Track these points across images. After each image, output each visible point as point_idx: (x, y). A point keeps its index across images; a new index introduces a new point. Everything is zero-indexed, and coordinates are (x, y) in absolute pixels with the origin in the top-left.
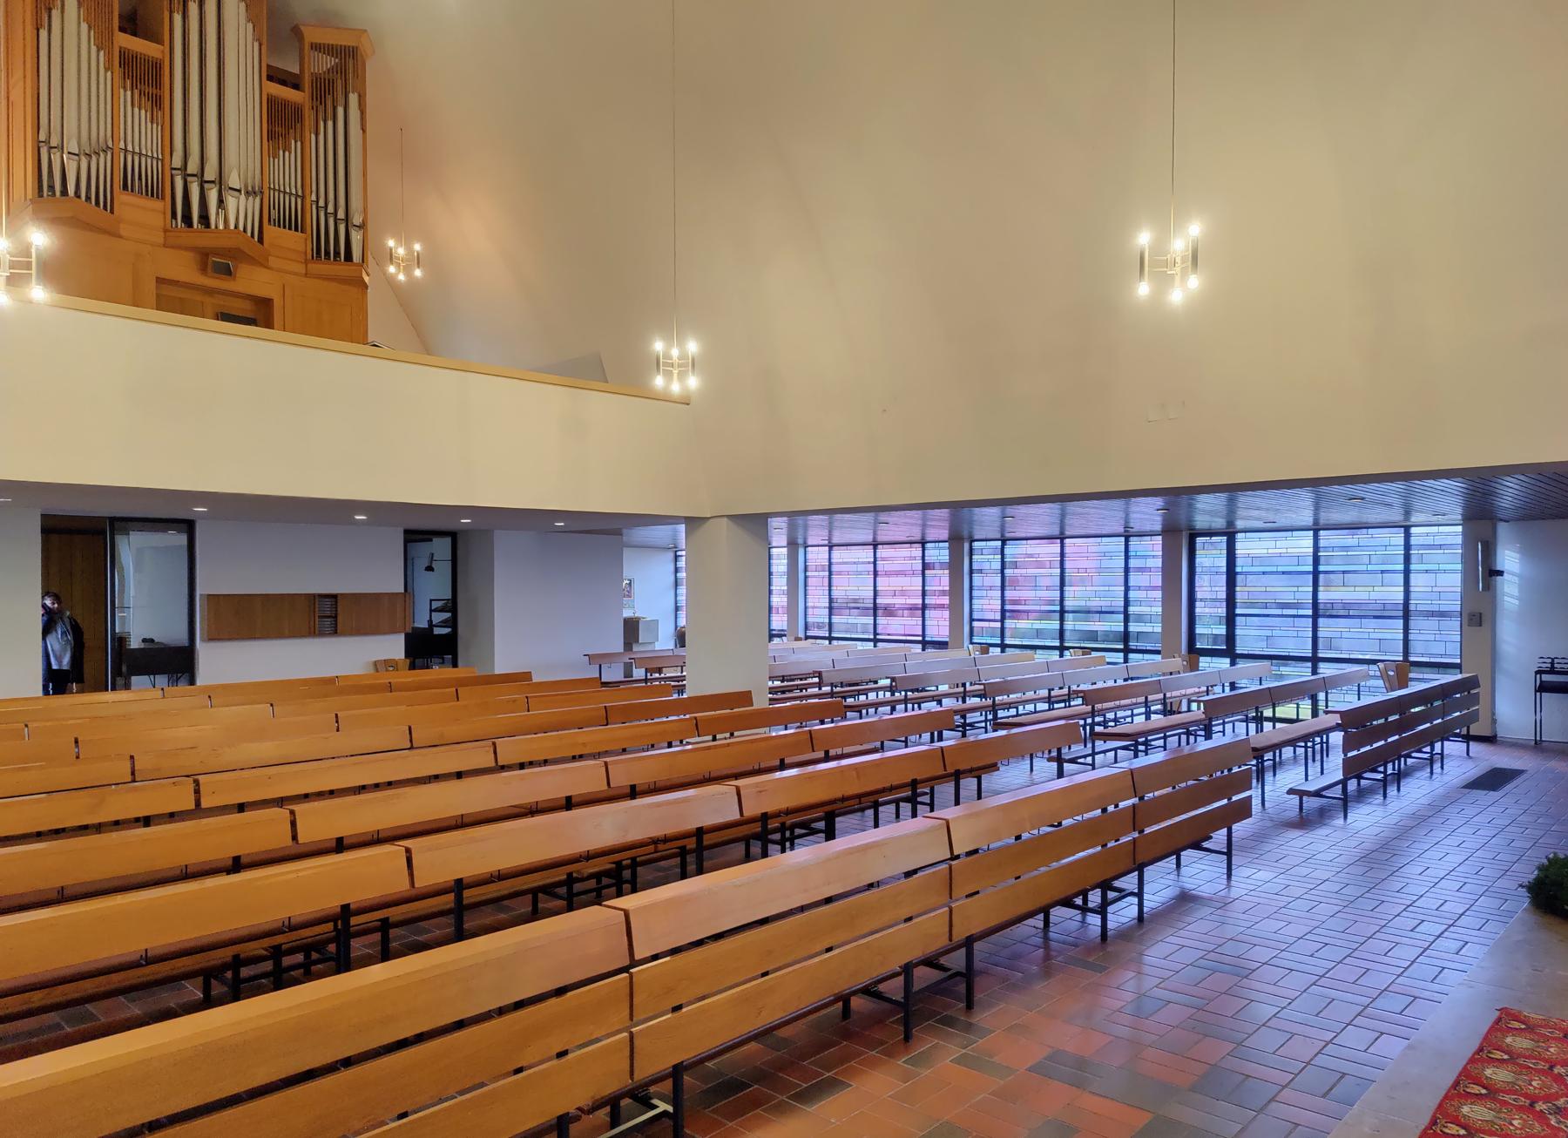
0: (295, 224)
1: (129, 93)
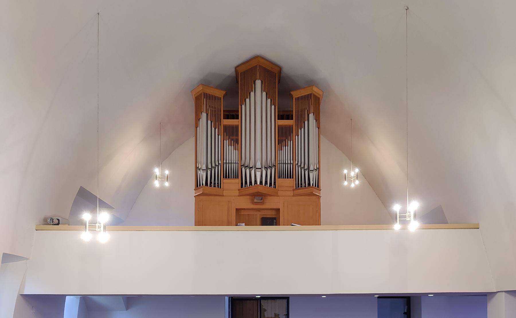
0: (290, 176)
1: (227, 141)
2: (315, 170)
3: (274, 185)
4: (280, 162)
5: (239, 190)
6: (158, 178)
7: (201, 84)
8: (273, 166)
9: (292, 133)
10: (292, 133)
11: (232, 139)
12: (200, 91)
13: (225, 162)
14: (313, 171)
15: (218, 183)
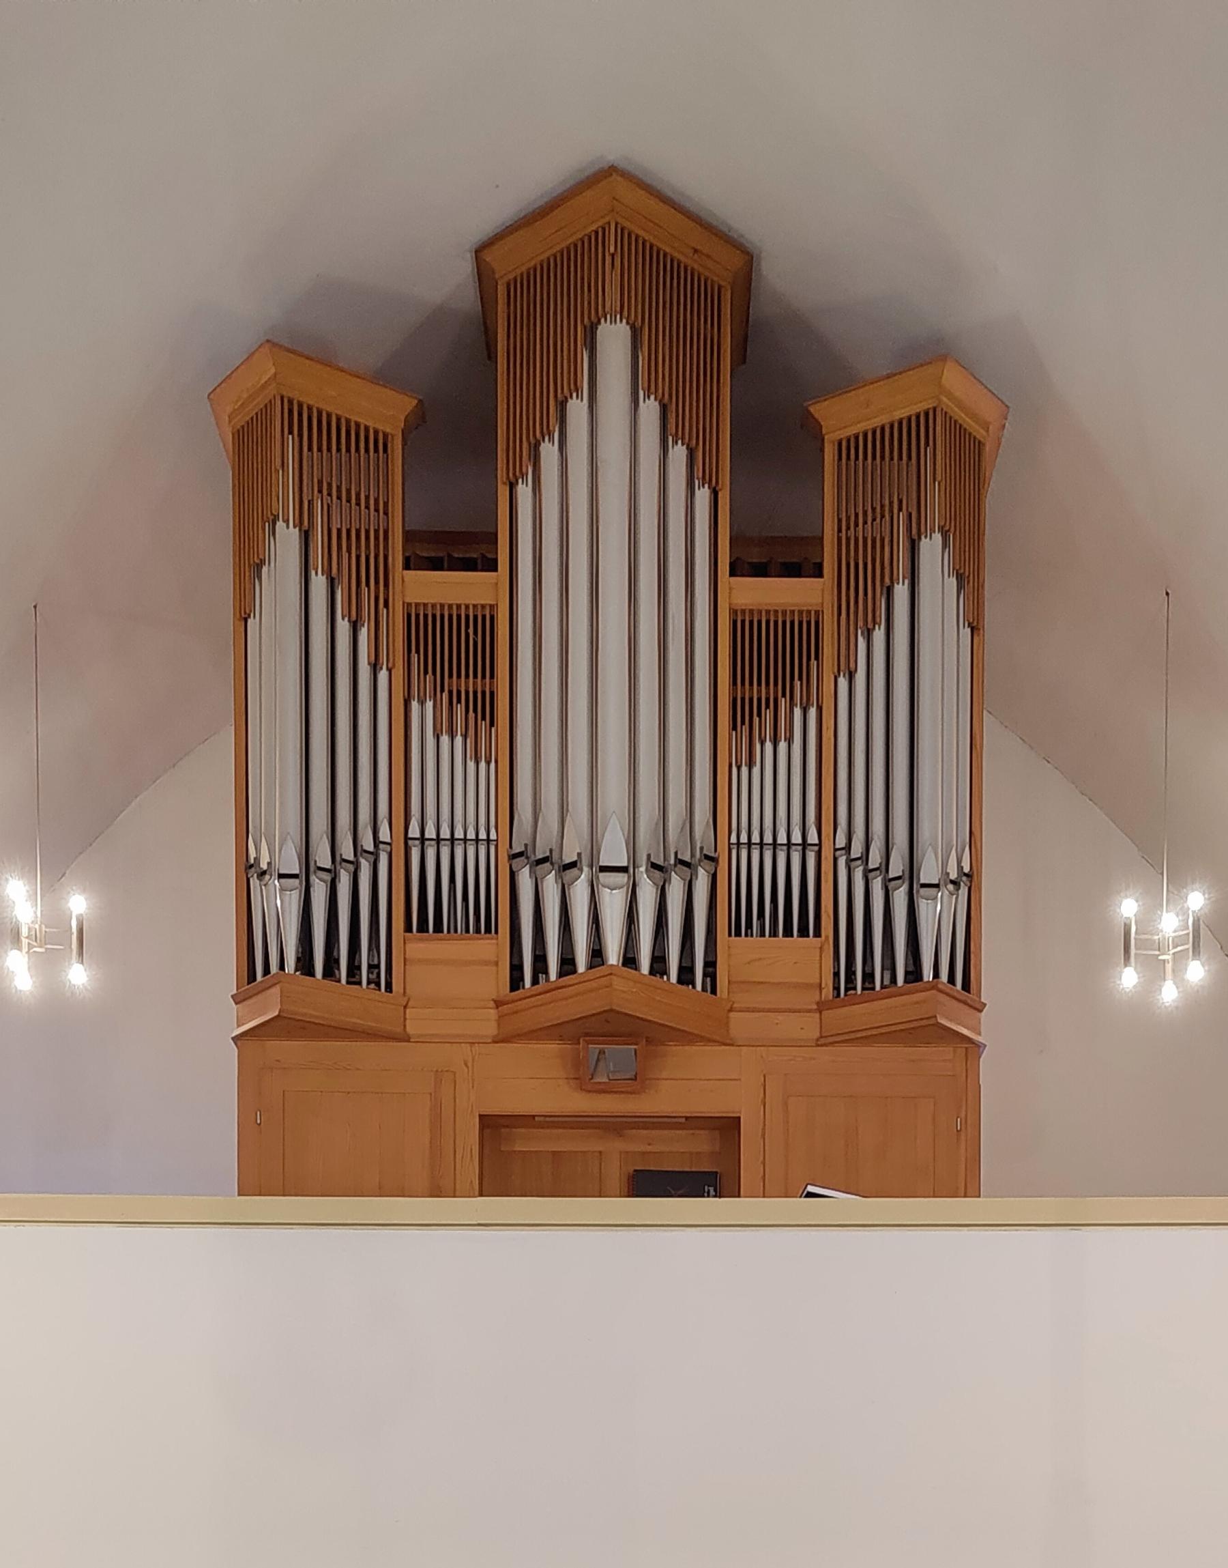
1: (429, 705)
2: (951, 887)
3: (705, 975)
4: (744, 839)
5: (498, 1004)
6: (25, 941)
7: (268, 341)
8: (700, 861)
9: (817, 658)
10: (817, 658)
11: (459, 692)
12: (264, 387)
13: (414, 831)
14: (937, 886)
15: (373, 967)
